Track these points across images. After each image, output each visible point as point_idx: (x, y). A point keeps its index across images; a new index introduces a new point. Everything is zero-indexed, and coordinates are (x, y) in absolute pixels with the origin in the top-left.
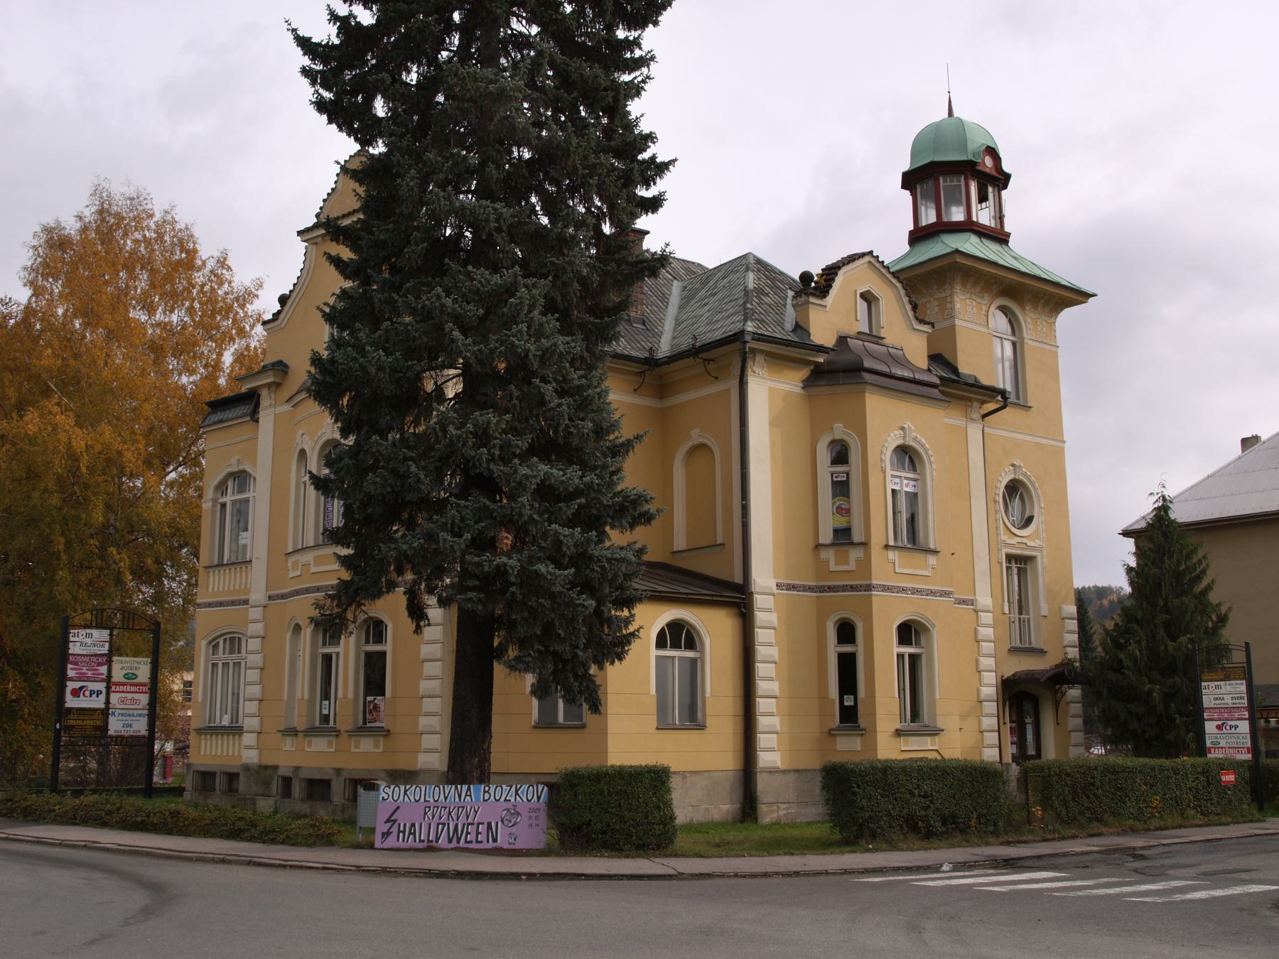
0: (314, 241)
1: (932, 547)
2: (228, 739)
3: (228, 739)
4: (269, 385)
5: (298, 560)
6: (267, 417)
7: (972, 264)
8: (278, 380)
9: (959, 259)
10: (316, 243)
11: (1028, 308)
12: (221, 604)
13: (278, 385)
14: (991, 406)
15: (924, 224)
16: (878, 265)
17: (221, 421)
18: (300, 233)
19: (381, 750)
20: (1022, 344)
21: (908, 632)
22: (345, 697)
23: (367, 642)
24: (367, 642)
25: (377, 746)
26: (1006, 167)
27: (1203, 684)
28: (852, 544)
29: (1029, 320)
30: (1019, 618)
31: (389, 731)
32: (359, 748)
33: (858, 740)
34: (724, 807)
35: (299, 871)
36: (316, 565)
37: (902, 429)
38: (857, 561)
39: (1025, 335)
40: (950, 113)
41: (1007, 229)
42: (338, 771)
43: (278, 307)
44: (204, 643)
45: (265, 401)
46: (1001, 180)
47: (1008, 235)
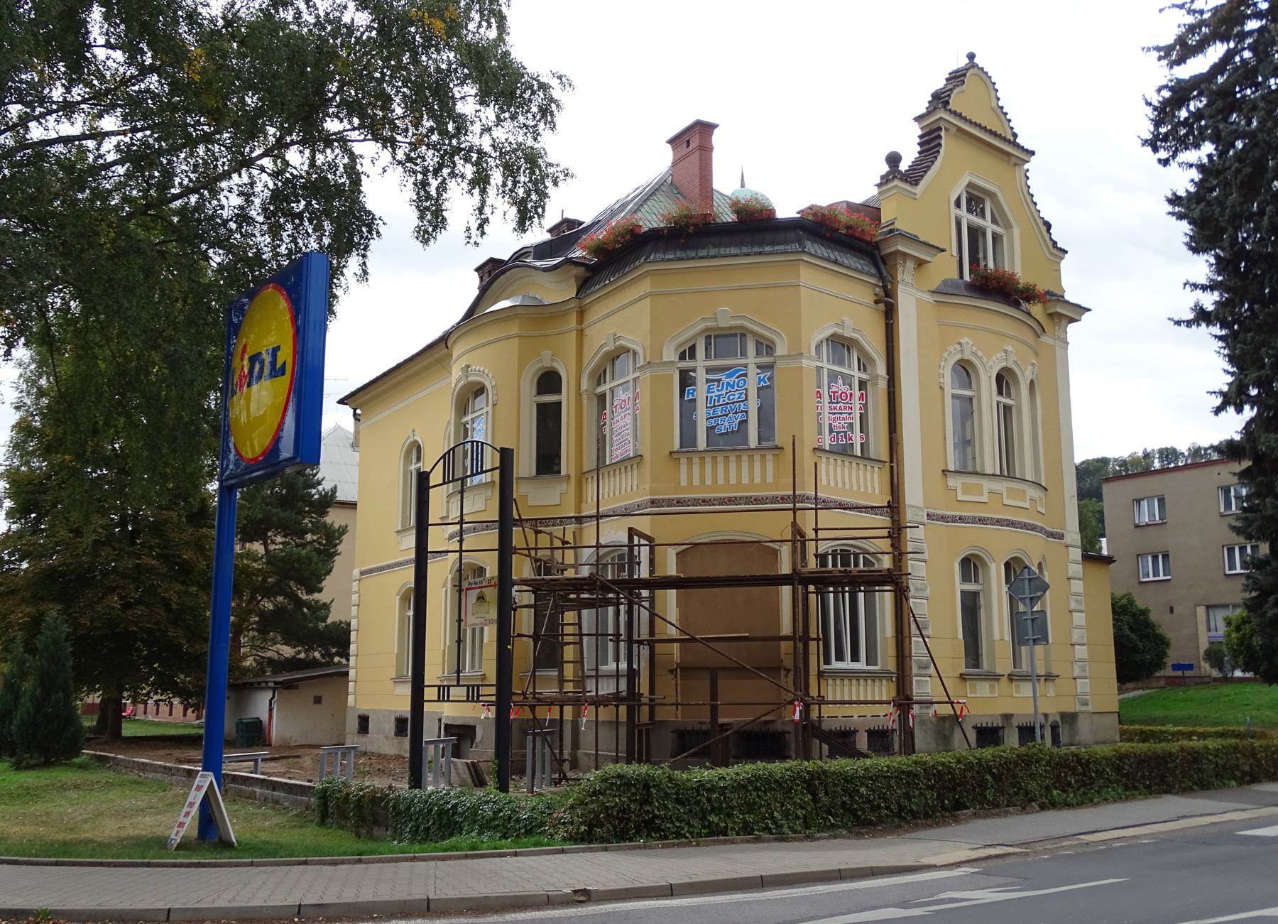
36: (964, 493)
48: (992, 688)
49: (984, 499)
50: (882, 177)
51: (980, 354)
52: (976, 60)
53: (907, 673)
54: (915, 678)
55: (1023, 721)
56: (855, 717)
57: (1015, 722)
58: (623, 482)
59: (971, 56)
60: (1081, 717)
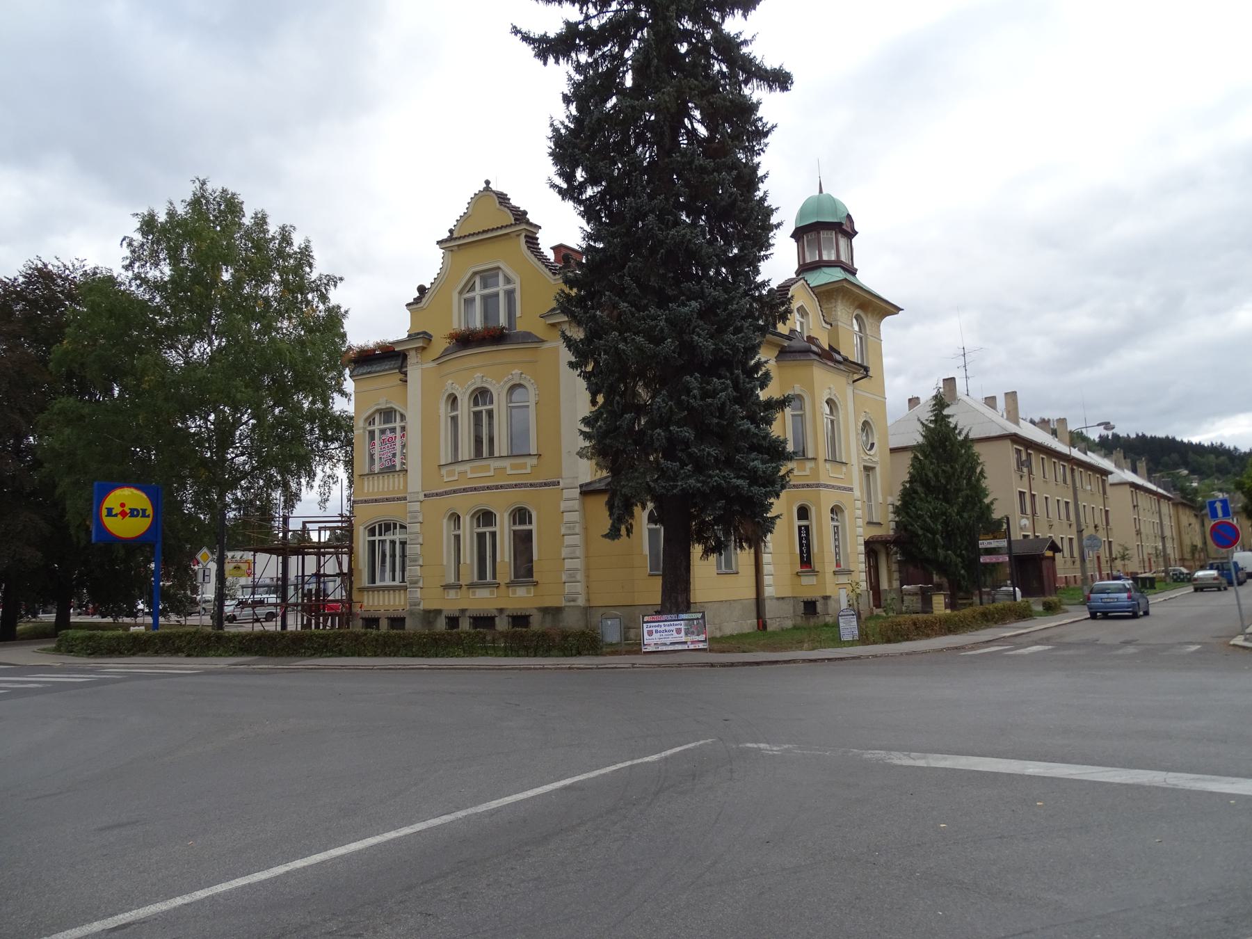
0: (450, 249)
1: (844, 461)
2: (389, 595)
3: (389, 595)
4: (416, 349)
5: (455, 470)
6: (415, 371)
7: (850, 287)
8: (425, 346)
9: (845, 284)
10: (452, 251)
11: (869, 315)
12: (376, 501)
13: (424, 348)
14: (856, 377)
15: (809, 261)
16: (807, 286)
17: (369, 373)
18: (438, 243)
19: (532, 595)
20: (867, 338)
21: (836, 510)
22: (502, 561)
23: (514, 523)
24: (514, 523)
25: (528, 592)
26: (856, 228)
27: (980, 542)
28: (808, 459)
29: (869, 321)
30: (372, 544)
31: (537, 582)
32: (475, 595)
33: (815, 578)
34: (749, 624)
35: (655, 655)
36: (512, 469)
37: (830, 388)
38: (811, 468)
39: (868, 332)
40: (821, 191)
41: (855, 266)
42: (501, 611)
43: (417, 294)
44: (361, 528)
45: (412, 358)
46: (850, 234)
47: (856, 270)
48: (457, 593)
49: (492, 473)
50: (414, 299)
51: (506, 379)
52: (490, 186)
53: (760, 562)
54: (661, 573)
55: (451, 614)
56: (382, 611)
57: (467, 614)
58: (376, 484)
59: (487, 182)
60: (566, 609)
